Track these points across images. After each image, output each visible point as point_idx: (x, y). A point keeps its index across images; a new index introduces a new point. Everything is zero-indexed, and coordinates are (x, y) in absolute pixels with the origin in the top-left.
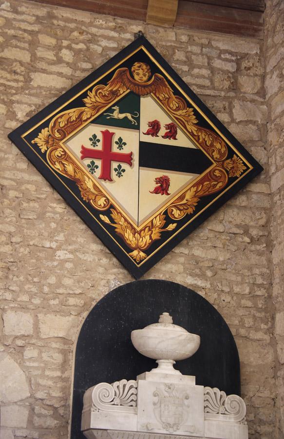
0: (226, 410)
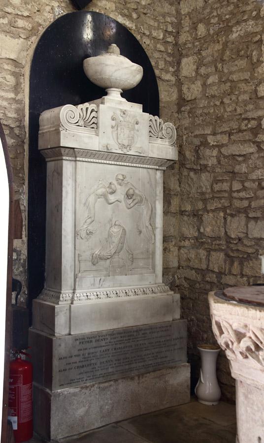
0: (163, 135)
